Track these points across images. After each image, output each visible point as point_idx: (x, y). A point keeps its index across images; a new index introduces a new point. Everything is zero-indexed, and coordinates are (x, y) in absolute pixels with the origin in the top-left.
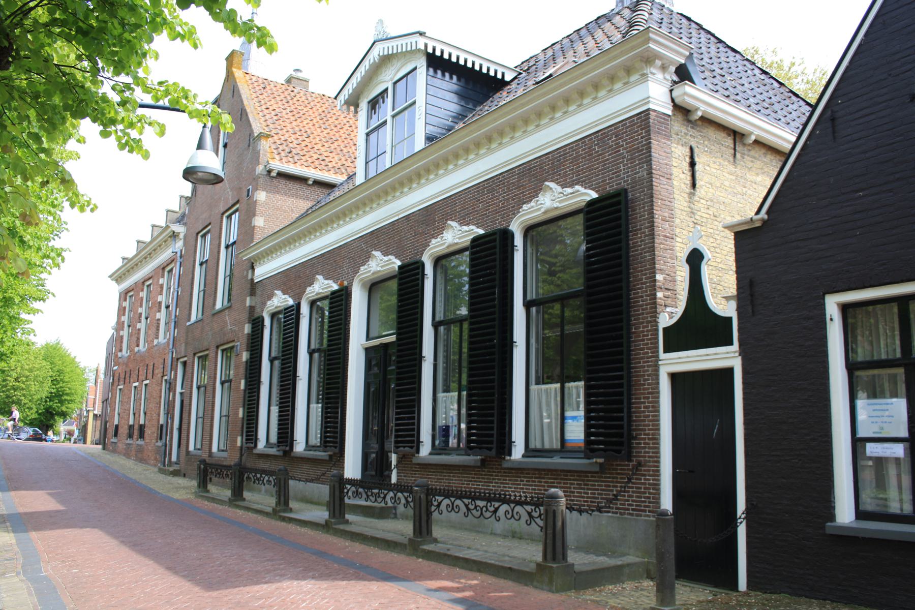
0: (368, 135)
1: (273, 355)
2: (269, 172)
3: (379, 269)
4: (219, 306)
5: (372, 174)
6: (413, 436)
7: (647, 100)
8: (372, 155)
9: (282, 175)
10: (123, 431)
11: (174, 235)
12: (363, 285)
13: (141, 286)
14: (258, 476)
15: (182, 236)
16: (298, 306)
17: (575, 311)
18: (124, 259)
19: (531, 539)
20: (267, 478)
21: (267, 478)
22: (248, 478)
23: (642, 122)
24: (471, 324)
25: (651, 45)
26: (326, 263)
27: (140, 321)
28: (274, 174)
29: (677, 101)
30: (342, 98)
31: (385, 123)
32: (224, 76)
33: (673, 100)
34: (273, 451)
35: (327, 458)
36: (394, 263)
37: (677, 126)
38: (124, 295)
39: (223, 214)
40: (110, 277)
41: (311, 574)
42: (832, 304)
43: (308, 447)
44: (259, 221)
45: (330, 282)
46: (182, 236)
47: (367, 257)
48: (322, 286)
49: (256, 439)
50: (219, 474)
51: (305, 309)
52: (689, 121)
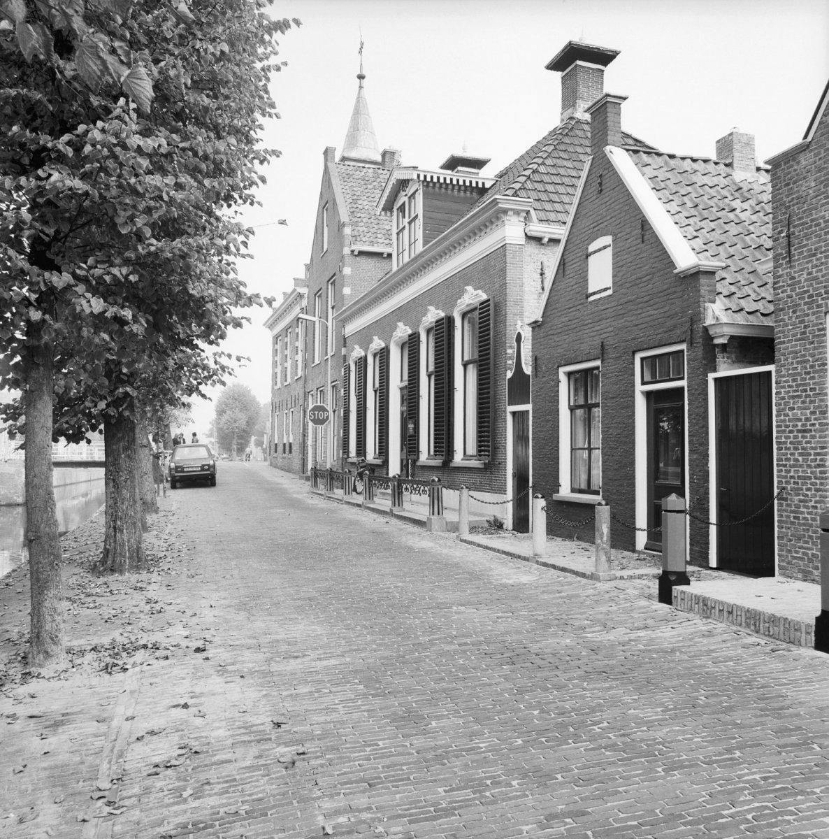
0: (398, 234)
1: (466, 358)
2: (353, 251)
3: (471, 302)
4: (317, 362)
5: (413, 256)
6: (415, 448)
7: (504, 238)
8: (413, 241)
9: (361, 253)
10: (280, 448)
11: (300, 296)
12: (397, 344)
13: (295, 322)
14: (415, 486)
15: (306, 296)
16: (366, 356)
17: (406, 392)
18: (284, 294)
19: (424, 504)
20: (422, 488)
21: (422, 488)
22: (406, 489)
23: (502, 251)
24: (436, 376)
25: (500, 205)
26: (401, 313)
27: (286, 361)
28: (356, 253)
29: (528, 234)
30: (381, 206)
31: (416, 217)
32: (323, 168)
33: (526, 234)
34: (475, 463)
35: (482, 466)
36: (481, 296)
37: (532, 248)
38: (276, 339)
39: (328, 281)
40: (264, 325)
41: (723, 667)
42: (683, 347)
43: (466, 456)
44: (347, 291)
45: (480, 292)
46: (306, 296)
47: (461, 293)
48: (433, 314)
49: (418, 452)
50: (415, 490)
51: (370, 360)
52: (543, 244)
